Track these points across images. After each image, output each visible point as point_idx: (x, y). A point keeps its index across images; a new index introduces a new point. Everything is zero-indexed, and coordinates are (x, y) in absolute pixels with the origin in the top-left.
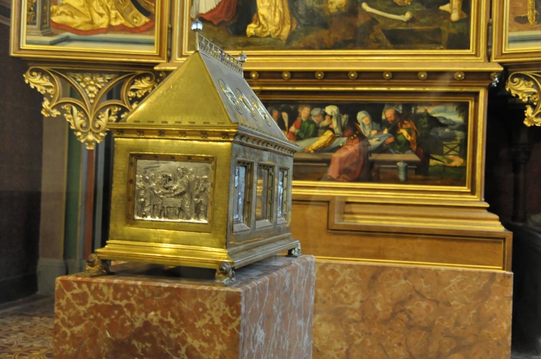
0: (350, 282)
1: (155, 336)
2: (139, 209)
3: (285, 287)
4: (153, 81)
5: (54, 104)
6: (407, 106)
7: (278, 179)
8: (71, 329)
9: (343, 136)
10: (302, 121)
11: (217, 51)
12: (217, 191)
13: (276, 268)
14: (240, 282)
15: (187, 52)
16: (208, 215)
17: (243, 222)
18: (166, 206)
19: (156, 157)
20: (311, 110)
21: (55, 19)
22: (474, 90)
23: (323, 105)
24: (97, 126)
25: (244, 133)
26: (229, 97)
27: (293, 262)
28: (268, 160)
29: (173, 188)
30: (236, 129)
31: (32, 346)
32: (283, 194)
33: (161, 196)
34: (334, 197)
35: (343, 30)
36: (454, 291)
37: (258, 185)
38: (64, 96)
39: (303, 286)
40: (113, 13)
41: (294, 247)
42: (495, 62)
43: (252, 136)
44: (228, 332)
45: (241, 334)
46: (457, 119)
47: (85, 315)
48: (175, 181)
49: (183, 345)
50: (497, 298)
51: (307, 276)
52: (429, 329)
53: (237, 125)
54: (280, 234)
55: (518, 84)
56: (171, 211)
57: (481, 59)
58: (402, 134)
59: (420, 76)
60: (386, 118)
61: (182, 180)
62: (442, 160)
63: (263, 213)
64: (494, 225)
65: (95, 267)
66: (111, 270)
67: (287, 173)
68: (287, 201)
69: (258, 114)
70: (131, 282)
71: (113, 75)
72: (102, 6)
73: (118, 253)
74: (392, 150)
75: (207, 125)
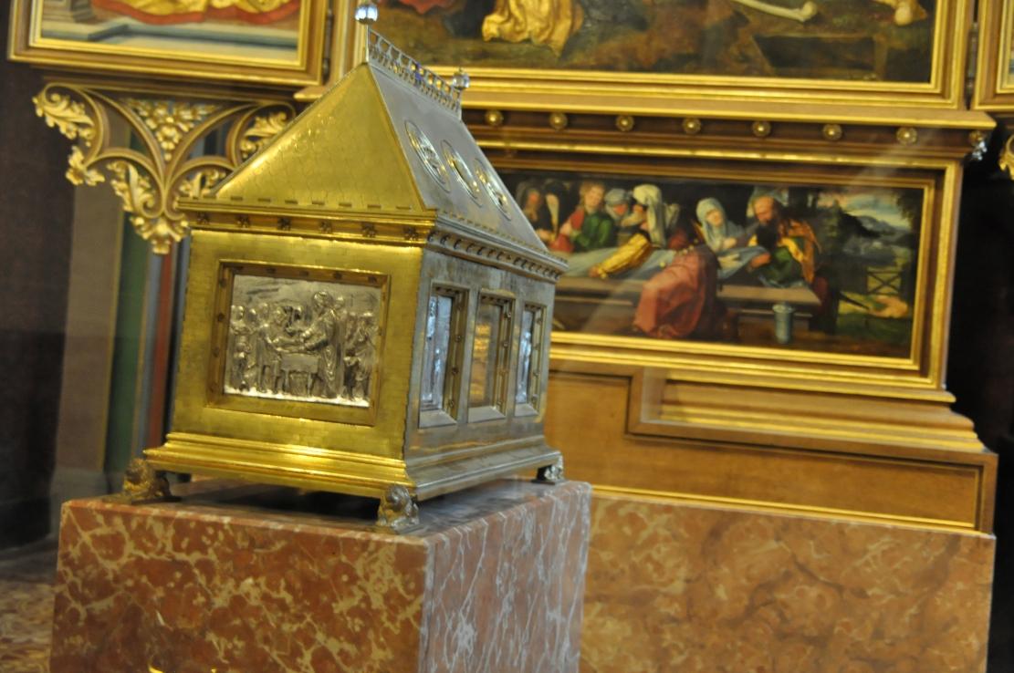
0: (666, 540)
2: (235, 374)
3: (523, 542)
5: (92, 160)
7: (521, 327)
8: (89, 606)
9: (667, 247)
10: (586, 214)
11: (406, 64)
12: (389, 344)
13: (507, 505)
16: (370, 391)
17: (443, 409)
18: (287, 370)
19: (272, 271)
23: (629, 184)
25: (449, 229)
26: (426, 158)
27: (546, 494)
28: (501, 287)
29: (304, 335)
30: (433, 221)
31: (29, 641)
32: (531, 356)
33: (279, 349)
34: (642, 369)
35: (677, 34)
36: (875, 567)
37: (476, 336)
38: (114, 142)
39: (564, 543)
41: (549, 464)
42: (979, 111)
43: (465, 238)
44: (398, 624)
45: (424, 630)
46: (899, 222)
47: (117, 579)
48: (308, 321)
51: (573, 524)
52: (821, 641)
53: (434, 213)
54: (519, 438)
56: (299, 380)
57: (952, 104)
58: (785, 248)
59: (827, 132)
61: (321, 319)
62: (865, 304)
63: (486, 392)
64: (964, 440)
65: (142, 485)
67: (542, 315)
68: (538, 370)
70: (209, 517)
71: (213, 106)
73: (188, 459)
74: (763, 280)
75: (348, 209)
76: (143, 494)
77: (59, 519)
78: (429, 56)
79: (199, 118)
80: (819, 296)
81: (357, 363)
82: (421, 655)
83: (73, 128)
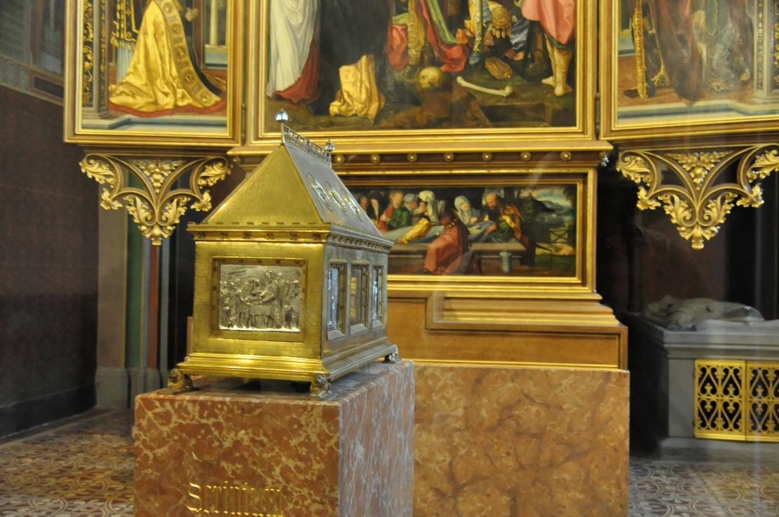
0: (452, 386)
1: (246, 456)
3: (384, 397)
4: (226, 167)
5: (115, 195)
6: (509, 190)
8: (154, 452)
9: (440, 224)
10: (394, 209)
12: (309, 297)
13: (374, 377)
14: (336, 395)
15: (263, 134)
19: (241, 261)
20: (403, 197)
21: (114, 100)
23: (417, 191)
24: (164, 218)
26: (319, 193)
30: (329, 229)
31: (94, 468)
32: (377, 294)
33: (248, 303)
34: (431, 293)
44: (326, 449)
45: (340, 451)
47: (169, 436)
49: (277, 465)
50: (612, 399)
52: (540, 436)
55: (630, 163)
58: (504, 221)
60: (487, 204)
64: (608, 319)
66: (195, 385)
69: (347, 207)
72: (167, 84)
74: (494, 239)
76: (180, 388)
77: (134, 406)
78: (301, 127)
79: (174, 168)
80: (524, 245)
81: (292, 308)
82: (340, 465)
83: (103, 178)
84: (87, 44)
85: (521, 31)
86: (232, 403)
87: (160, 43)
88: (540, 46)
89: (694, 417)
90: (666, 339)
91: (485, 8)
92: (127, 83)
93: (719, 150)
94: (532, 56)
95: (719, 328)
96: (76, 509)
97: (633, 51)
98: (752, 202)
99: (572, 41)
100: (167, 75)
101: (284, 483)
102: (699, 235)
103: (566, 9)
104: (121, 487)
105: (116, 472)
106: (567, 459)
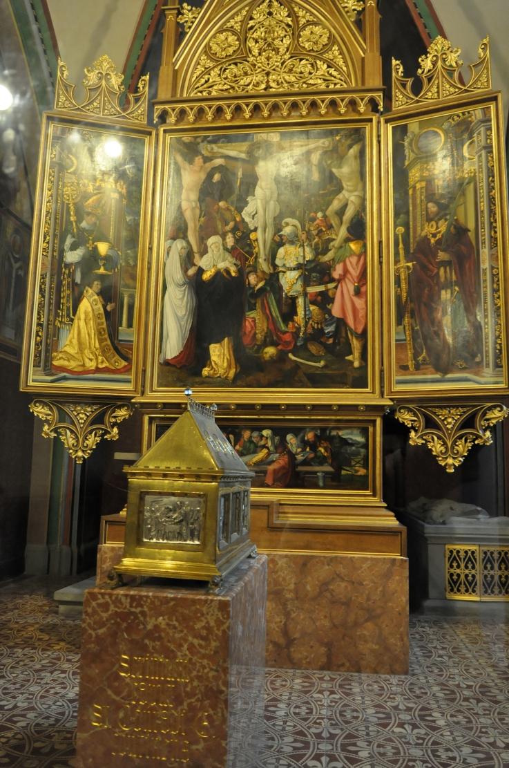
9: (276, 453)
19: (160, 494)
21: (55, 363)
22: (372, 418)
23: (260, 429)
24: (85, 445)
40: (100, 358)
46: (360, 439)
50: (397, 578)
52: (347, 604)
58: (320, 451)
64: (392, 520)
78: (182, 384)
80: (333, 467)
84: (39, 325)
85: (331, 325)
86: (154, 597)
87: (89, 326)
88: (344, 335)
89: (445, 585)
90: (426, 531)
91: (307, 309)
92: (65, 351)
93: (462, 407)
94: (339, 340)
95: (461, 522)
96: (15, 656)
97: (405, 340)
98: (485, 441)
99: (365, 331)
100: (92, 347)
101: (190, 656)
102: (451, 463)
103: (361, 311)
104: (46, 637)
105: (42, 625)
106: (367, 621)
